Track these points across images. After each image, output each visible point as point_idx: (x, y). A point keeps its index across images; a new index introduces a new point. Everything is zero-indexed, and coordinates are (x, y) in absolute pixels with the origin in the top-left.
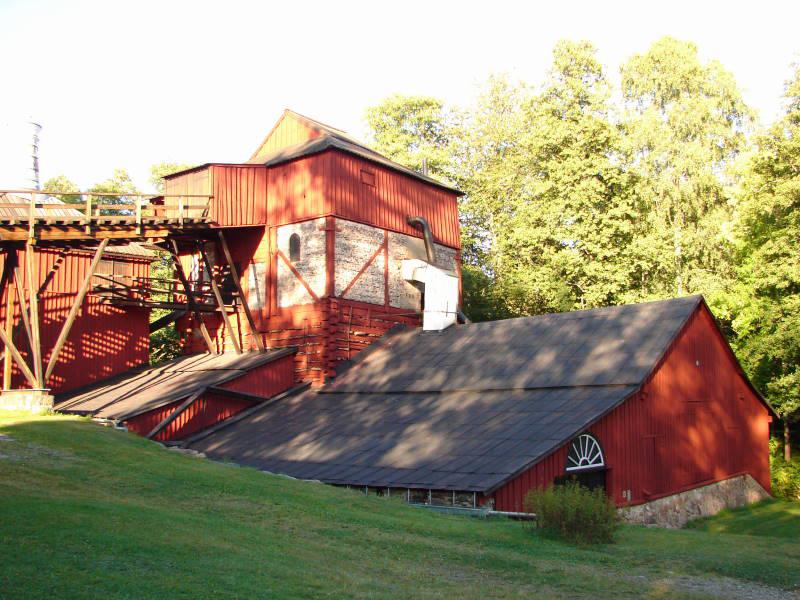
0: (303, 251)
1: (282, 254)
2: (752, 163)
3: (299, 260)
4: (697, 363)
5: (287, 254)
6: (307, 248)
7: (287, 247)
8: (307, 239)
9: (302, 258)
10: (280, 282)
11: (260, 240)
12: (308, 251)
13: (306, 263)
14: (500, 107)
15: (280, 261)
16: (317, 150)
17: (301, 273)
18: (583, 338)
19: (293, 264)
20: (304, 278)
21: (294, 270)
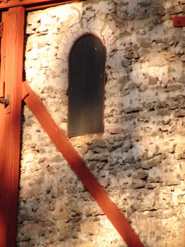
0: (113, 101)
1: (39, 108)
2: (107, 92)
3: (100, 129)
4: (56, 130)
5: (58, 112)
6: (128, 86)
7: (60, 84)
8: (132, 58)
9: (109, 125)
10: (27, 206)
11: (117, 229)
12: (134, 100)
13: (125, 141)
14: (57, 63)
15: (34, 133)
16: (17, 5)
17: (104, 177)
18: (164, 165)
19: (79, 143)
20: (117, 199)
21: (78, 166)
